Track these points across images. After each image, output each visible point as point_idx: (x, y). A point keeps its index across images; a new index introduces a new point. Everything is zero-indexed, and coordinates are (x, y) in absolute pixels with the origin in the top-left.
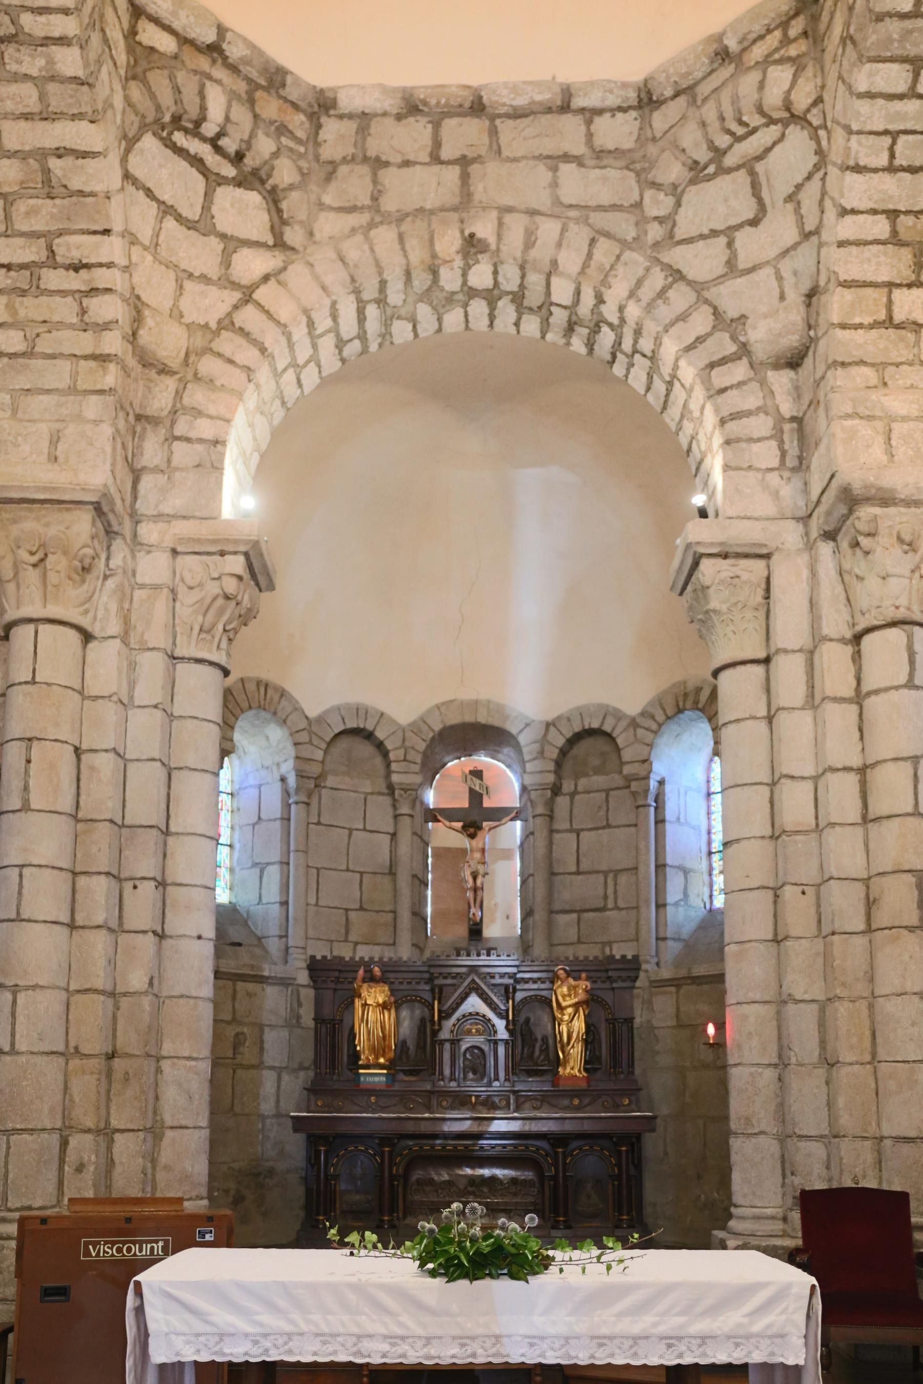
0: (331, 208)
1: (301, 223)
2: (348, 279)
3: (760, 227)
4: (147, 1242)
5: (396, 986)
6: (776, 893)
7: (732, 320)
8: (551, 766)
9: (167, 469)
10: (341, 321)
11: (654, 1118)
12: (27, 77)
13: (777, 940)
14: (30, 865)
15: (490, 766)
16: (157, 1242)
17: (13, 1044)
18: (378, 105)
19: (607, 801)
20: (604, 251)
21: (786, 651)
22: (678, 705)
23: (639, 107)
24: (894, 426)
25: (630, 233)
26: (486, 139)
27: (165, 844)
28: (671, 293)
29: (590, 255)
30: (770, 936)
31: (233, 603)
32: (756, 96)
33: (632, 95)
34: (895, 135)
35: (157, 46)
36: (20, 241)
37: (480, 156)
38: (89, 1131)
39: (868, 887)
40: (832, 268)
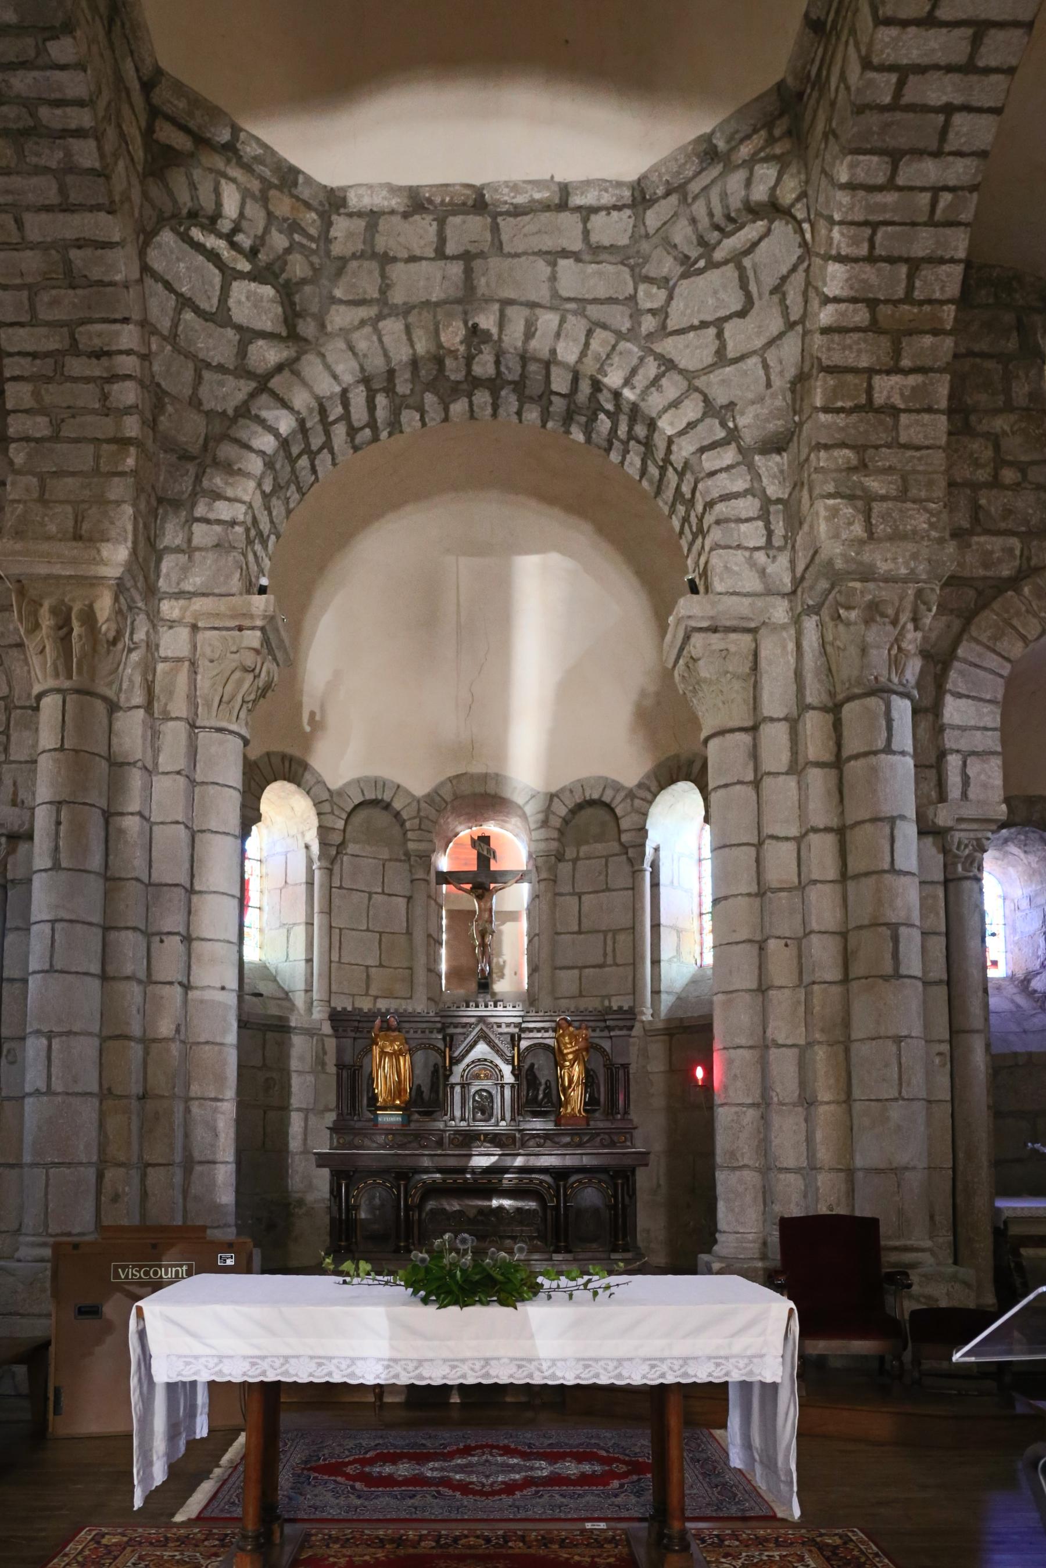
0: (341, 302)
1: (313, 315)
2: (357, 367)
3: (748, 318)
4: (172, 1266)
5: (411, 1034)
7: (722, 407)
8: (555, 834)
9: (189, 549)
10: (352, 410)
11: (647, 1153)
12: (46, 170)
15: (498, 836)
16: (181, 1266)
18: (386, 203)
20: (600, 341)
21: (772, 720)
23: (633, 206)
24: (874, 504)
25: (625, 325)
26: (488, 236)
28: (664, 381)
29: (587, 345)
30: (754, 986)
31: (251, 676)
32: (743, 193)
33: (627, 193)
34: (875, 226)
35: (174, 144)
36: (43, 330)
37: (482, 252)
40: (815, 354)
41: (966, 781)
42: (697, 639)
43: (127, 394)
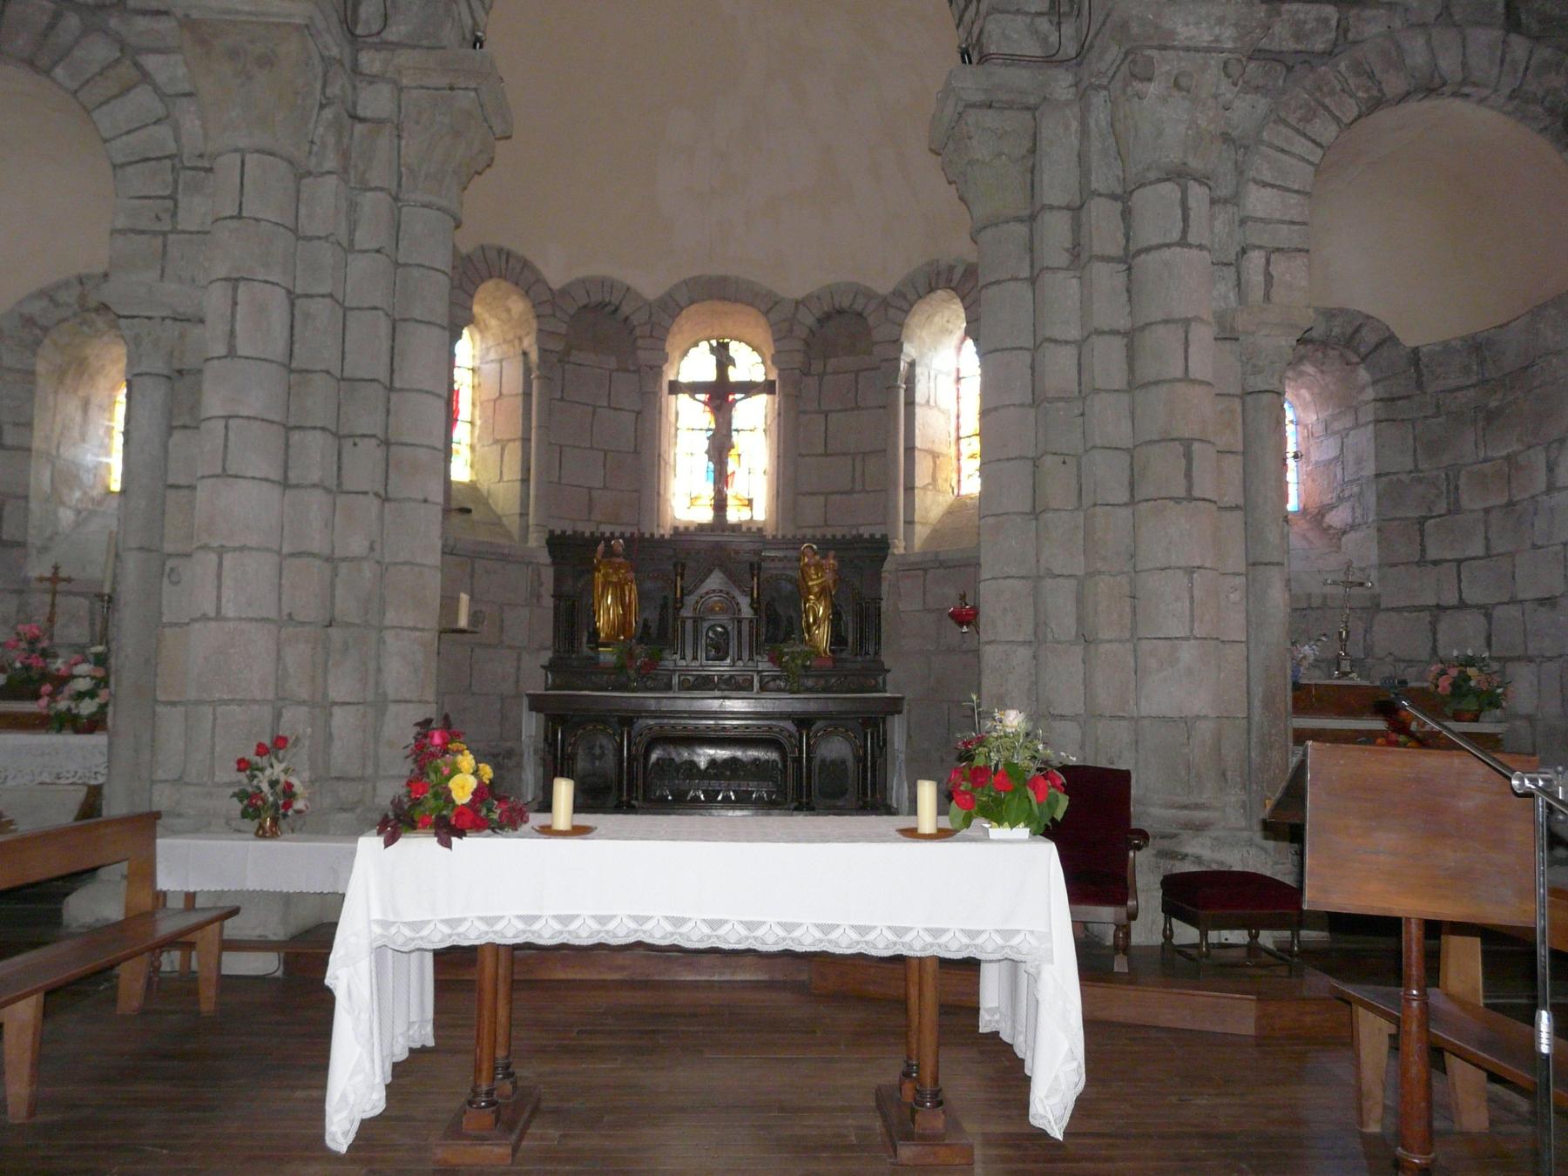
6: (1036, 462)
11: (902, 699)
13: (1035, 513)
14: (237, 417)
17: (219, 608)
19: (857, 382)
21: (1051, 208)
22: (930, 284)
27: (388, 400)
30: (1027, 508)
38: (304, 703)
39: (1132, 457)
41: (1269, 277)
42: (972, 117)
43: (567, 655)
